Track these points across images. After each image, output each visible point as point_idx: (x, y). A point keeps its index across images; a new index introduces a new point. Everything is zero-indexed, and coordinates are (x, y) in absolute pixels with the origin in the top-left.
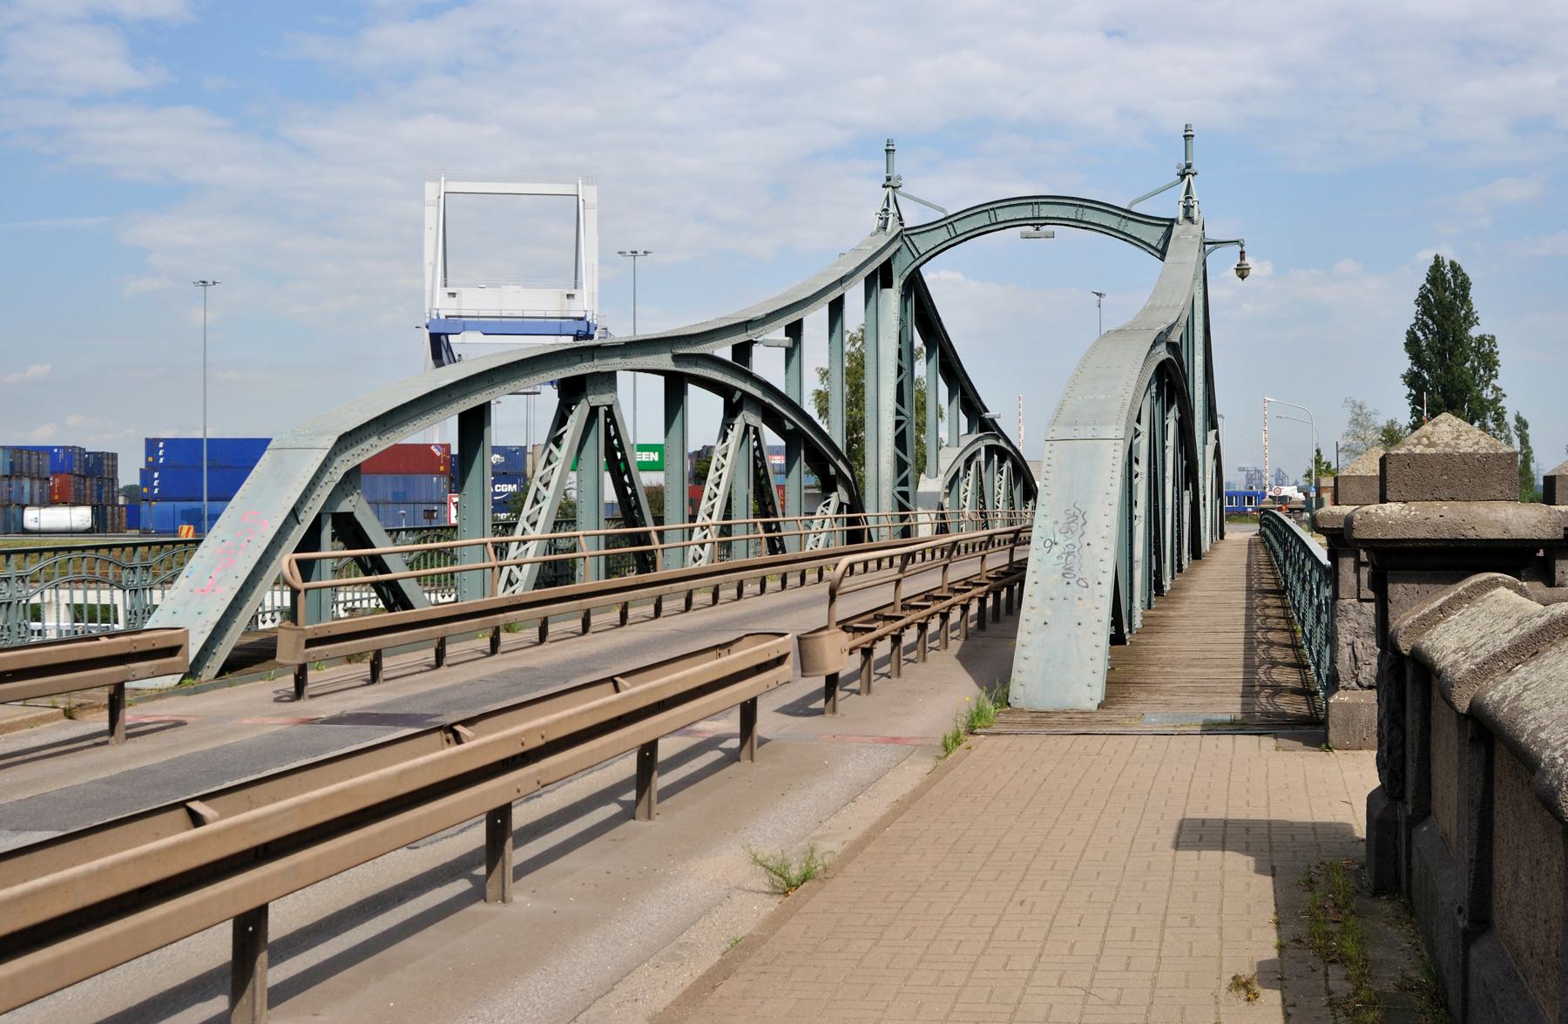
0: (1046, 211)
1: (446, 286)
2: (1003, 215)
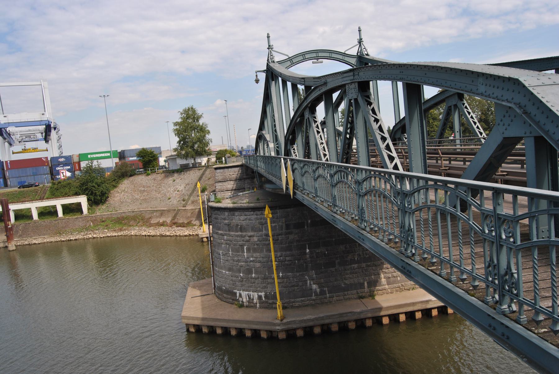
0: (320, 54)
1: (3, 114)
2: (307, 56)
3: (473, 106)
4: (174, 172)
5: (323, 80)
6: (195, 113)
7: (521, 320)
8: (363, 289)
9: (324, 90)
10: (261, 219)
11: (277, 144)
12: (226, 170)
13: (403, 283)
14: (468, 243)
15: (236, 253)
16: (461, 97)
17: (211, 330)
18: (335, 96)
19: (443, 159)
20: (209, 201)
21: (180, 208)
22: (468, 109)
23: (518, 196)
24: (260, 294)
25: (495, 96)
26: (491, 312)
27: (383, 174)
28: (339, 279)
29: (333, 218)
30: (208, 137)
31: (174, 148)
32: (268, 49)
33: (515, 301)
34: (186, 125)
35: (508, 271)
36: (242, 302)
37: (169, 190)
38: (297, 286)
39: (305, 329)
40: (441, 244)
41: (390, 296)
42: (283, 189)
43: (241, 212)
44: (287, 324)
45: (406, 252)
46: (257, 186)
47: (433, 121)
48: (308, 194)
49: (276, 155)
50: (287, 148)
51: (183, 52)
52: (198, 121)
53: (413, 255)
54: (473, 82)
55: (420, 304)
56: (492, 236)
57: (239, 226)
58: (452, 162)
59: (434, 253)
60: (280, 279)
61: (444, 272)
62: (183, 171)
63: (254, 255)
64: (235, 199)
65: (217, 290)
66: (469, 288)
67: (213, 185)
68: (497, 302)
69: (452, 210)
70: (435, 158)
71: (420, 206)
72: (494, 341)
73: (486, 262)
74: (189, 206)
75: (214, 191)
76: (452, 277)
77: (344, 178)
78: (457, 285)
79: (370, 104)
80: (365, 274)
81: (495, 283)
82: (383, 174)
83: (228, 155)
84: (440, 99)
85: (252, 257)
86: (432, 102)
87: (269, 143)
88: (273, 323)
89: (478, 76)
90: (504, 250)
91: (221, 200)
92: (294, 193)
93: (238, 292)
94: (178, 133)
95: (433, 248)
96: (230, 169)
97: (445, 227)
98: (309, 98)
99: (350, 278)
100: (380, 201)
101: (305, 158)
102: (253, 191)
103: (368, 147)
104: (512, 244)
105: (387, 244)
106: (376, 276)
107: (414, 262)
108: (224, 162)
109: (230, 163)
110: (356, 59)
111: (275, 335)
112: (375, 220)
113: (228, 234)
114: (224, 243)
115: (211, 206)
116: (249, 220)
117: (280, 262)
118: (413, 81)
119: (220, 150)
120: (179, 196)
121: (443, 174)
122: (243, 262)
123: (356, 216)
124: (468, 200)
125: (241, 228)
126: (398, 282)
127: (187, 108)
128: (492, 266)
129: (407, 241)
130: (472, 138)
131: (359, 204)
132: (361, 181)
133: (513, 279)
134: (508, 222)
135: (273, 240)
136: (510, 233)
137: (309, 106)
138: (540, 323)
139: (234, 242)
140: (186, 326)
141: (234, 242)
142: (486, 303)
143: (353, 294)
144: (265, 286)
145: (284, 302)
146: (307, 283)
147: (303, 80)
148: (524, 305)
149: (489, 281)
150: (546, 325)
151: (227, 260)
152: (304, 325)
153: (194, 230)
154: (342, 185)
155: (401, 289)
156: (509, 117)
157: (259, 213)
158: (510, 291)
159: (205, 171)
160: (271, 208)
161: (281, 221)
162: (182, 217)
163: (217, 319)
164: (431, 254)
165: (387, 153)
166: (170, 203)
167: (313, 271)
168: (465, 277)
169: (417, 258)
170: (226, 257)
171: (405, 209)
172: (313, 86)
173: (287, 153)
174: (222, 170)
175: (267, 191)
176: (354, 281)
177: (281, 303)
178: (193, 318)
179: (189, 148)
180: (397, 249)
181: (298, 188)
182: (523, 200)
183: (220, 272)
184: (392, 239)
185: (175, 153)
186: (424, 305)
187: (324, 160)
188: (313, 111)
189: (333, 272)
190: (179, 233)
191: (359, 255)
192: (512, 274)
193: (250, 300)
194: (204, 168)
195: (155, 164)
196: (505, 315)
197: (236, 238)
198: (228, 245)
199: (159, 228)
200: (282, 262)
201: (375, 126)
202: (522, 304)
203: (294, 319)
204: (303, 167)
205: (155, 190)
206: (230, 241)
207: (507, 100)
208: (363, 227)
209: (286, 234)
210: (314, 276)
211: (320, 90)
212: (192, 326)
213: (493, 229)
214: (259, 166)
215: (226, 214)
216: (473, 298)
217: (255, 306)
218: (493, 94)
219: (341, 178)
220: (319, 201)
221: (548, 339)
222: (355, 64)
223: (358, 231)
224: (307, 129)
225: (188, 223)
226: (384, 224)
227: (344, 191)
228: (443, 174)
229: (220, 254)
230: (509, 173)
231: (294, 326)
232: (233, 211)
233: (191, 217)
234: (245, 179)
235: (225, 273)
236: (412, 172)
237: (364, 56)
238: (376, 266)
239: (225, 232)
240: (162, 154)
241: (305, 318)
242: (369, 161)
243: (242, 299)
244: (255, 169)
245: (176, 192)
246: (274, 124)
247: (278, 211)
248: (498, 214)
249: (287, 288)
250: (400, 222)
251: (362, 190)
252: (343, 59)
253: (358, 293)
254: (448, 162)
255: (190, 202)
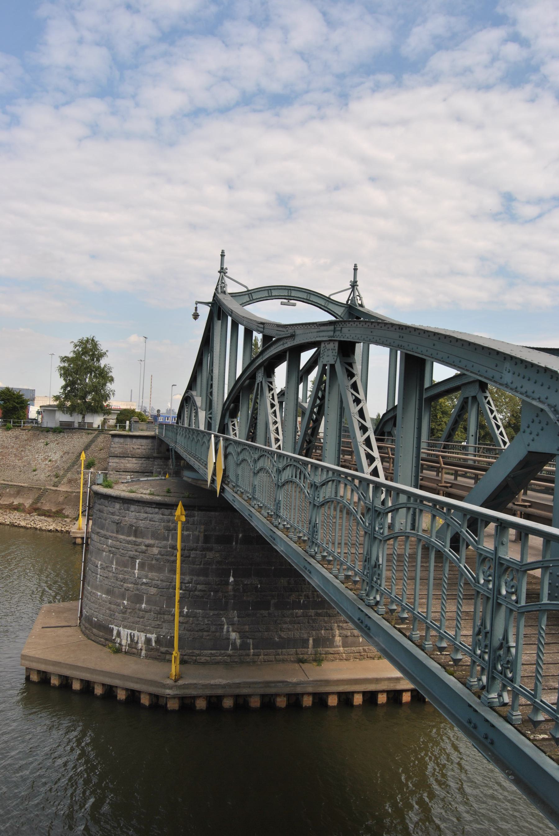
0: (294, 294)
2: (274, 293)
3: (500, 403)
4: (48, 430)
5: (290, 331)
6: (96, 348)
7: (514, 718)
8: (305, 648)
9: (290, 345)
10: (168, 521)
11: (211, 414)
12: (128, 440)
13: (366, 648)
14: (453, 597)
15: (123, 569)
16: (483, 387)
17: (64, 683)
18: (306, 357)
19: (444, 470)
20: (93, 483)
21: (48, 487)
22: (491, 406)
23: (530, 536)
24: (149, 635)
25: (523, 390)
26: (472, 700)
27: (349, 478)
28: (272, 628)
29: (272, 533)
30: (109, 386)
31: (55, 395)
32: (220, 272)
33: (509, 688)
34: (80, 363)
35: (504, 642)
36: (120, 644)
37: (37, 456)
38: (207, 631)
39: (209, 698)
40: (418, 592)
41: (344, 665)
42: (207, 481)
43: (140, 507)
44: (184, 688)
45: (367, 597)
46: (172, 471)
47: (442, 416)
48: (242, 493)
49: (207, 429)
50: (224, 422)
51: (94, 256)
52: (98, 360)
53: (377, 603)
54: (496, 366)
55: (386, 682)
56: (488, 589)
57: (134, 528)
58: (459, 478)
59: (406, 604)
60: (183, 616)
61: (417, 634)
62: (63, 432)
63: (150, 575)
64: (133, 485)
65: (83, 622)
66: (448, 662)
67: (105, 459)
68: (483, 688)
69: (439, 543)
70: (436, 469)
71: (396, 532)
72: (473, 745)
73: (476, 626)
74: (63, 486)
75: (106, 469)
76: (427, 643)
77: (296, 477)
78: (432, 656)
79: (351, 375)
80: (312, 626)
81: (483, 659)
82: (349, 478)
83: (135, 418)
84: (451, 386)
85: (146, 577)
86: (442, 389)
87: (199, 410)
88: (162, 683)
89: (505, 359)
90: (503, 609)
91: (113, 485)
92: (222, 489)
93: (115, 628)
94: (65, 373)
95: (405, 596)
96: (134, 440)
97: (426, 569)
98: (266, 353)
99: (289, 629)
100: (341, 518)
101: (247, 440)
102: (163, 478)
103: (340, 437)
104: (514, 603)
105: (343, 583)
106: (327, 631)
107: (377, 615)
108: (127, 428)
109: (136, 430)
110: (344, 308)
111: (162, 702)
112: (330, 544)
113: (115, 537)
114: (106, 550)
115: (97, 491)
116: (150, 520)
117: (187, 591)
118: (416, 353)
119: (125, 410)
120: (50, 468)
121: (441, 492)
122: (132, 583)
123: (304, 535)
124: (461, 532)
125: (136, 531)
126: (359, 645)
127: (85, 339)
128: (483, 634)
129: (371, 582)
130: (492, 447)
131: (311, 518)
132: (318, 485)
133: (509, 655)
134: (512, 570)
135: (182, 556)
136: (513, 587)
137: (265, 364)
138: (540, 724)
139: (123, 551)
140: (26, 671)
141: (123, 551)
142: (469, 688)
143: (289, 655)
144: (158, 625)
145: (184, 654)
146: (223, 628)
147: (262, 326)
148: (520, 696)
149: (477, 655)
150: (547, 730)
151: (106, 577)
152: (208, 692)
153: (64, 523)
154: (292, 487)
155: (361, 657)
156: (540, 423)
157: (167, 512)
158: (502, 673)
159: (96, 437)
160: (186, 507)
161: (198, 530)
162: (49, 501)
163: (77, 666)
164: (402, 605)
165: (365, 450)
166: (35, 478)
167: (235, 612)
168: (444, 644)
169: (382, 609)
170: (106, 571)
171: (374, 534)
172: (275, 337)
173: (223, 429)
174: (122, 440)
175: (184, 481)
176: (294, 634)
177: (179, 653)
178: (39, 660)
179: (78, 398)
180: (354, 592)
181: (229, 482)
182: (536, 541)
183: (94, 593)
184: (351, 575)
185: (56, 403)
186: (392, 685)
187: (274, 448)
188: (270, 373)
189: (265, 617)
190: (41, 525)
191: (307, 597)
192: (509, 648)
193: (133, 643)
194: (96, 432)
195: (22, 414)
196: (492, 708)
197: (127, 545)
198: (112, 554)
199: (10, 513)
200: (190, 591)
201: (354, 409)
202: (518, 694)
203: (195, 682)
204: (241, 452)
205: (15, 454)
206: (117, 548)
207: (539, 399)
208: (313, 553)
209: (203, 549)
210: (236, 619)
211: (283, 344)
212: (36, 673)
213: (490, 578)
214: (178, 441)
215: (117, 506)
216: (451, 677)
217: (138, 654)
218: (522, 387)
219: (292, 477)
220: (256, 507)
221: (546, 750)
222: (342, 316)
223: (304, 559)
224: (256, 398)
225: (57, 511)
226: (342, 553)
227: (293, 496)
228: (441, 492)
229: (97, 566)
230: (533, 505)
231: (194, 692)
232: (128, 503)
233: (63, 504)
234: (155, 458)
235: (101, 596)
236: (397, 482)
237: (356, 306)
238: (329, 616)
239: (111, 534)
240: (35, 401)
241: (212, 682)
242: (339, 457)
243: (121, 641)
244: (172, 445)
245: (47, 462)
246: (210, 383)
247: (196, 513)
248: (500, 557)
249: (193, 632)
250: (365, 553)
251: (318, 497)
252: (326, 306)
253: (297, 654)
254: (453, 477)
255: (65, 480)
